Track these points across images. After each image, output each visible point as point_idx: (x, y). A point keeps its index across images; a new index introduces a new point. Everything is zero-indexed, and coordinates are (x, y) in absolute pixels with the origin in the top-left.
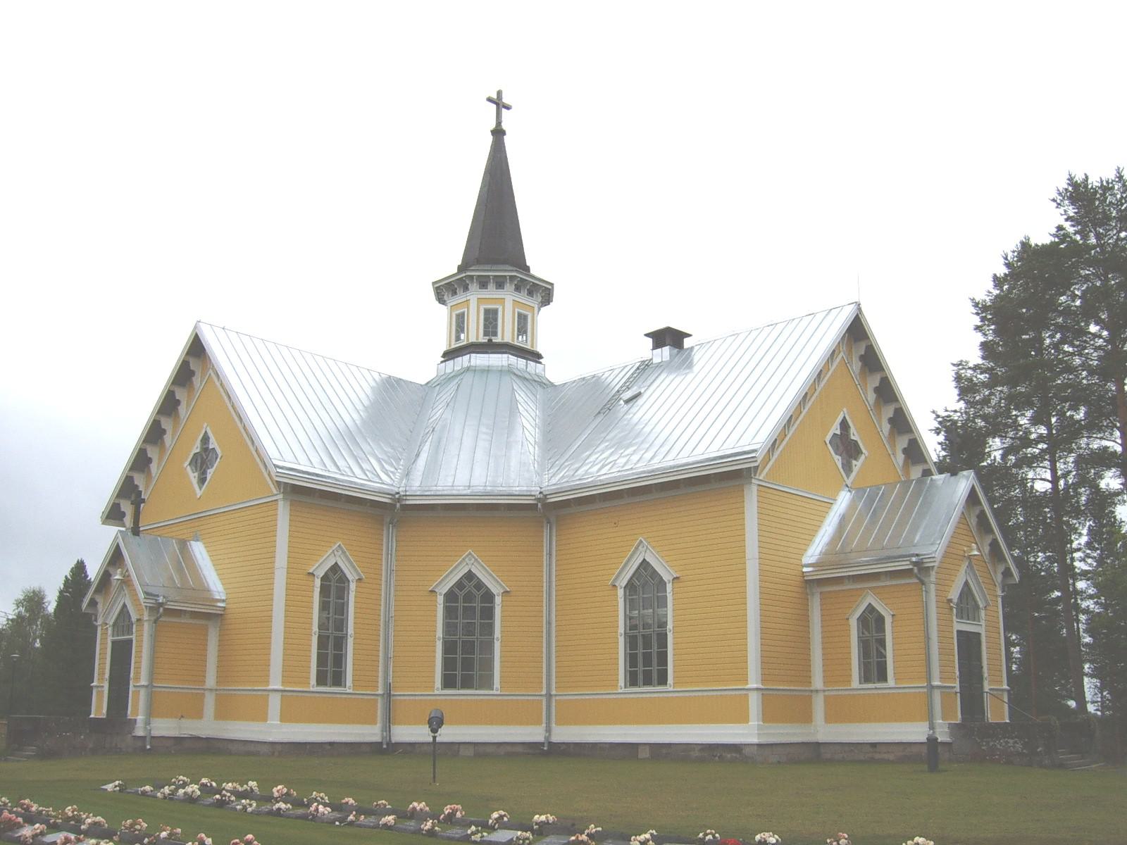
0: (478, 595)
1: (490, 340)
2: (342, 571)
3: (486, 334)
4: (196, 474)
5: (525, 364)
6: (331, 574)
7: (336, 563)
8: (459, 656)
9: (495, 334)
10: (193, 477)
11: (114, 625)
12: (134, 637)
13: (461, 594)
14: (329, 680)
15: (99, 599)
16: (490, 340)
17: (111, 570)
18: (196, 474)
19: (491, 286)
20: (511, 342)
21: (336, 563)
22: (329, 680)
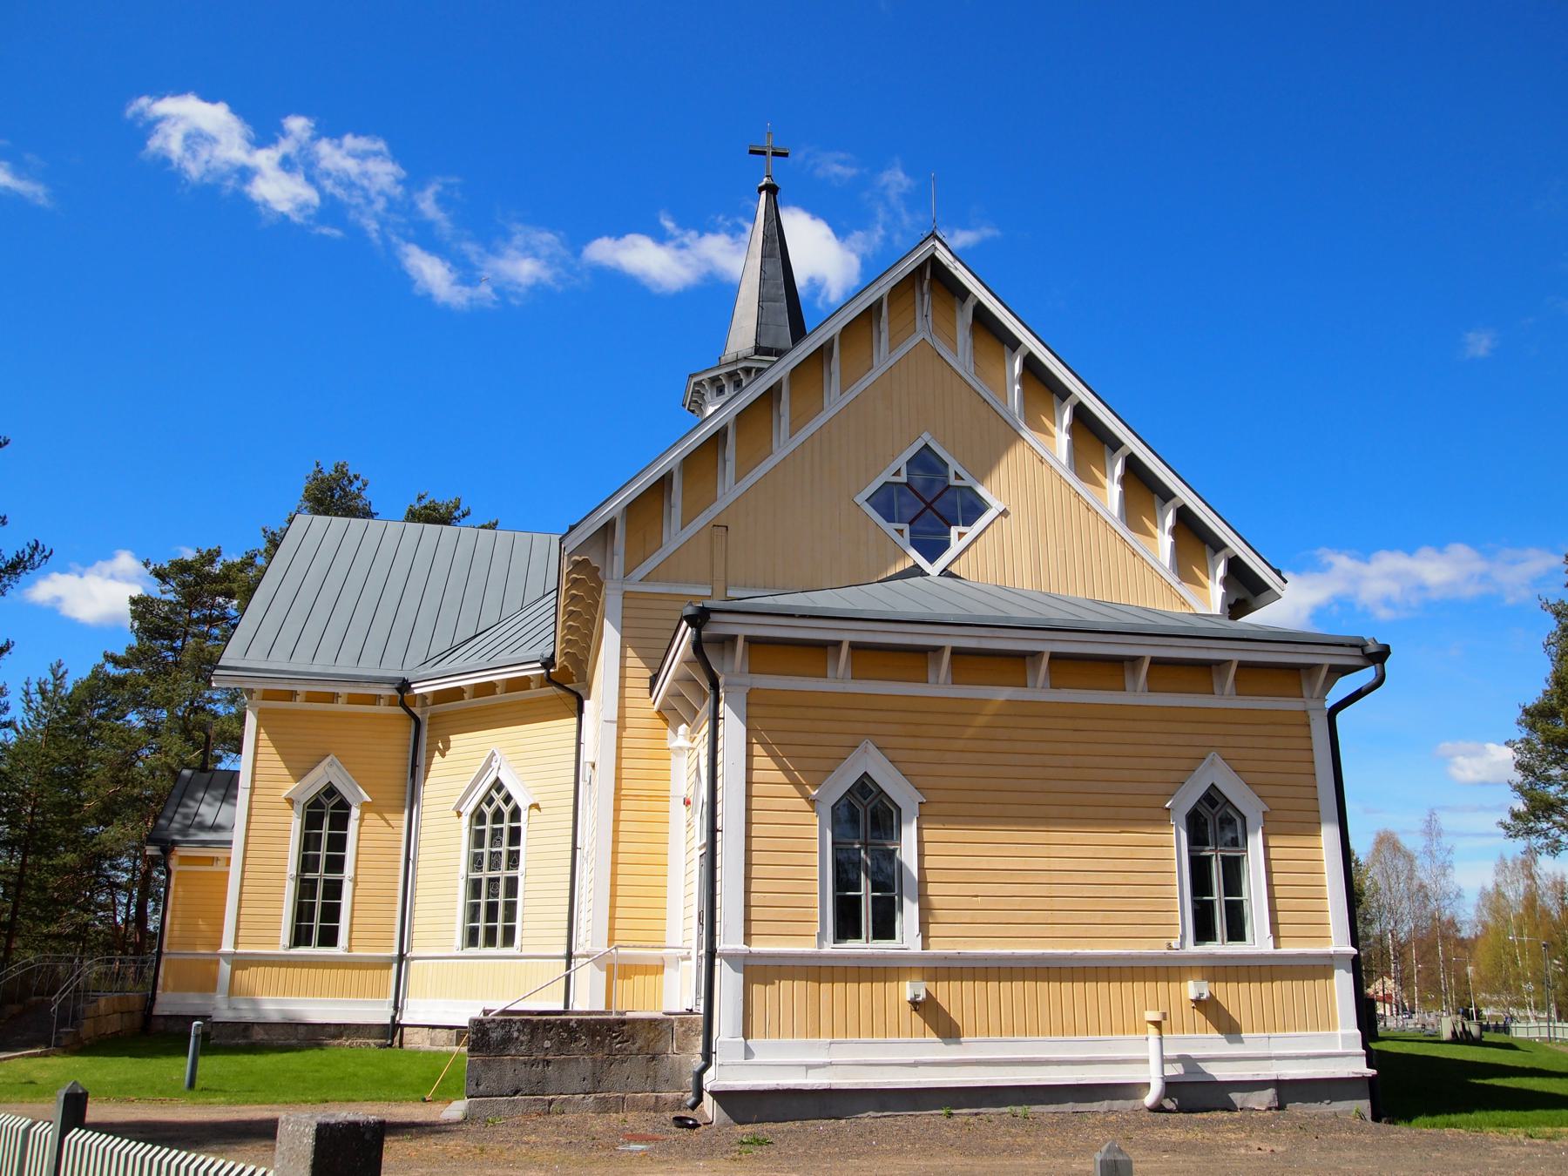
0: (507, 810)
13: (489, 811)
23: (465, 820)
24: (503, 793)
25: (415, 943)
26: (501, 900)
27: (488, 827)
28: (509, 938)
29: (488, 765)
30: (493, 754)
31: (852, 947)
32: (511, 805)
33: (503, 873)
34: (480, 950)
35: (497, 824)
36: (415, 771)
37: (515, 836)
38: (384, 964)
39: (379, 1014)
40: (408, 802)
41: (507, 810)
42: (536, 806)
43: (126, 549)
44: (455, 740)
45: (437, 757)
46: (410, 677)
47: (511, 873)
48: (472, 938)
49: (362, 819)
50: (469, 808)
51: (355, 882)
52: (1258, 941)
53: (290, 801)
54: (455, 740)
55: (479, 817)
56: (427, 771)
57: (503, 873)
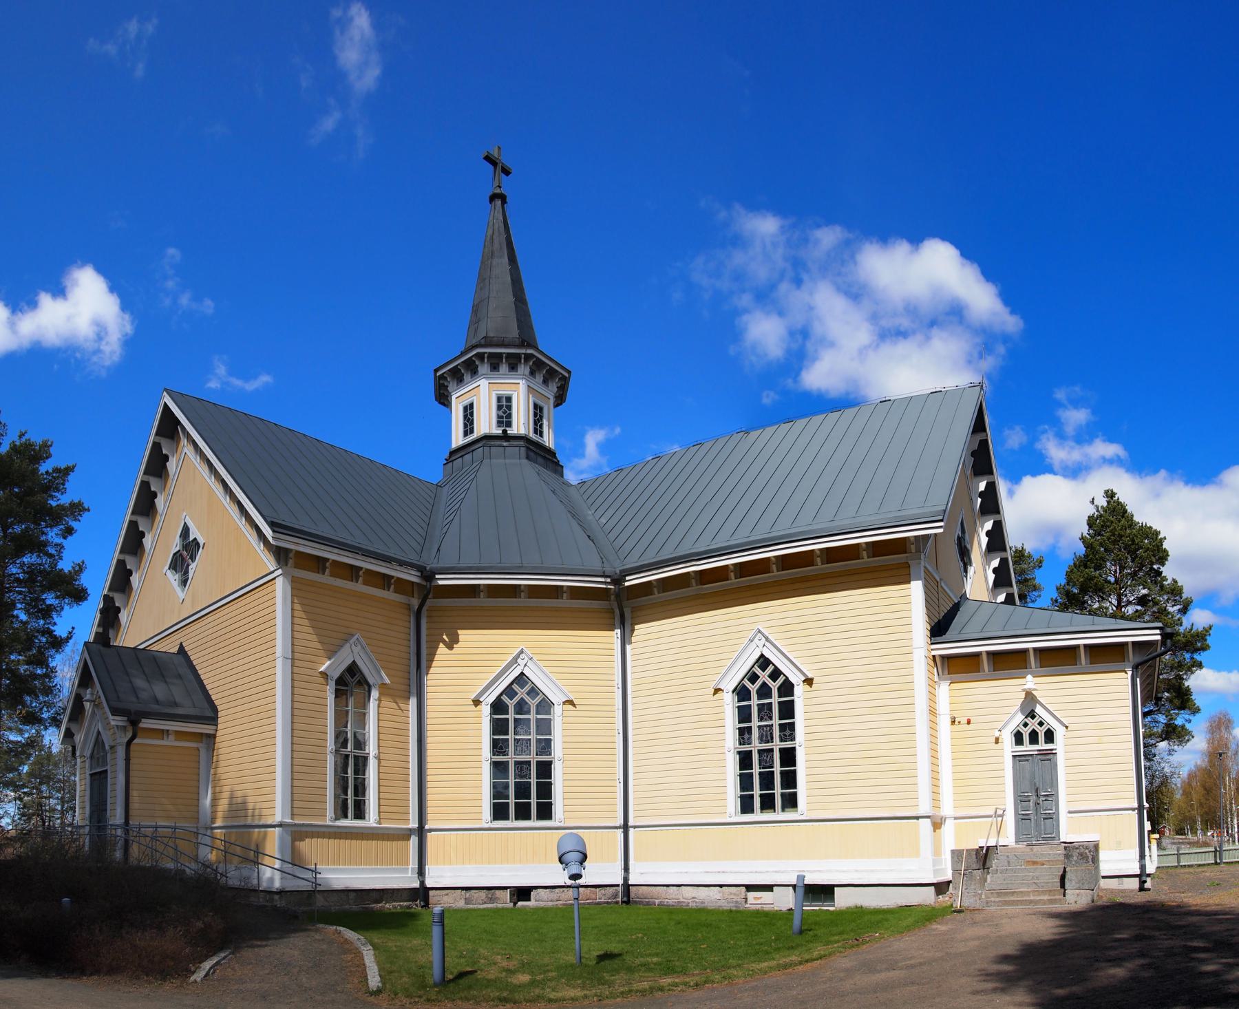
0: (774, 686)
1: (505, 431)
2: (362, 673)
3: (499, 423)
4: (177, 576)
5: (430, 869)
6: (348, 677)
7: (354, 662)
8: (534, 801)
9: (509, 424)
10: (173, 578)
11: (92, 757)
12: (108, 768)
13: (753, 688)
14: (350, 812)
15: (74, 728)
16: (505, 431)
17: (82, 692)
18: (177, 576)
19: (504, 368)
20: (532, 435)
21: (354, 662)
22: (350, 812)
23: (486, 709)
24: (770, 669)
25: (429, 817)
26: (777, 769)
27: (755, 702)
28: (791, 802)
29: (515, 660)
30: (522, 652)
31: (343, 823)
32: (781, 680)
33: (533, 758)
34: (758, 816)
35: (516, 715)
36: (420, 663)
37: (788, 710)
38: (404, 835)
39: (405, 879)
40: (414, 690)
41: (774, 686)
42: (571, 702)
43: (84, 263)
44: (463, 634)
45: (442, 649)
46: (431, 564)
47: (788, 744)
48: (499, 812)
49: (379, 700)
50: (730, 684)
51: (378, 758)
52: (372, 819)
53: (324, 675)
54: (463, 634)
55: (498, 707)
56: (429, 667)
57: (533, 758)
